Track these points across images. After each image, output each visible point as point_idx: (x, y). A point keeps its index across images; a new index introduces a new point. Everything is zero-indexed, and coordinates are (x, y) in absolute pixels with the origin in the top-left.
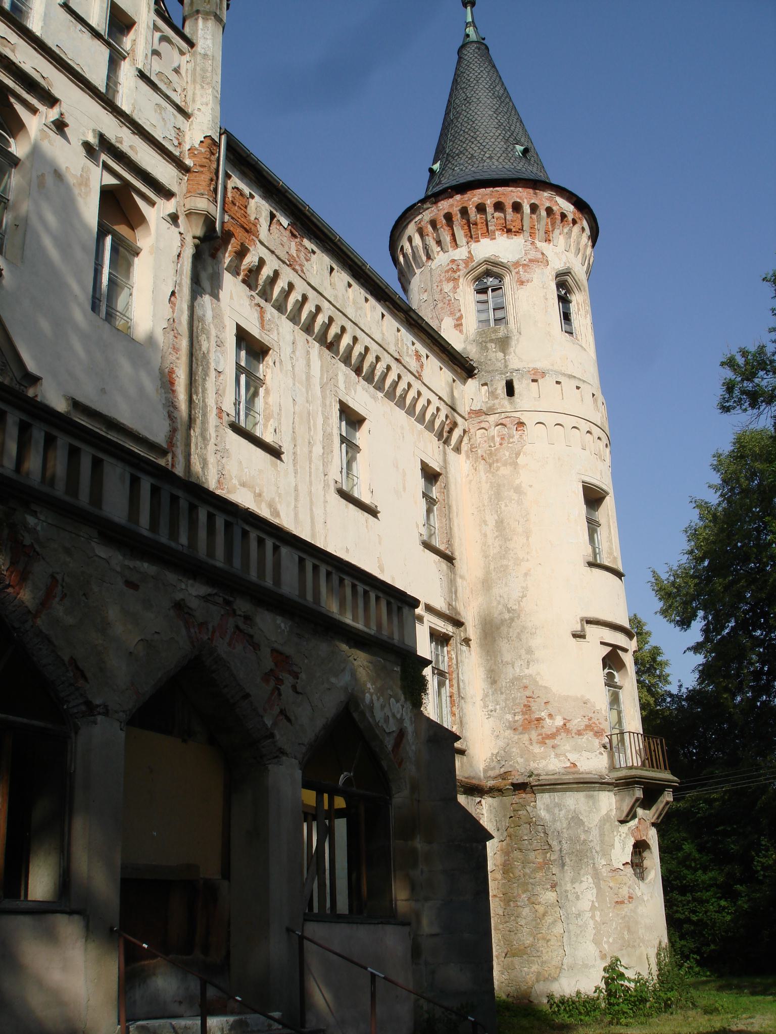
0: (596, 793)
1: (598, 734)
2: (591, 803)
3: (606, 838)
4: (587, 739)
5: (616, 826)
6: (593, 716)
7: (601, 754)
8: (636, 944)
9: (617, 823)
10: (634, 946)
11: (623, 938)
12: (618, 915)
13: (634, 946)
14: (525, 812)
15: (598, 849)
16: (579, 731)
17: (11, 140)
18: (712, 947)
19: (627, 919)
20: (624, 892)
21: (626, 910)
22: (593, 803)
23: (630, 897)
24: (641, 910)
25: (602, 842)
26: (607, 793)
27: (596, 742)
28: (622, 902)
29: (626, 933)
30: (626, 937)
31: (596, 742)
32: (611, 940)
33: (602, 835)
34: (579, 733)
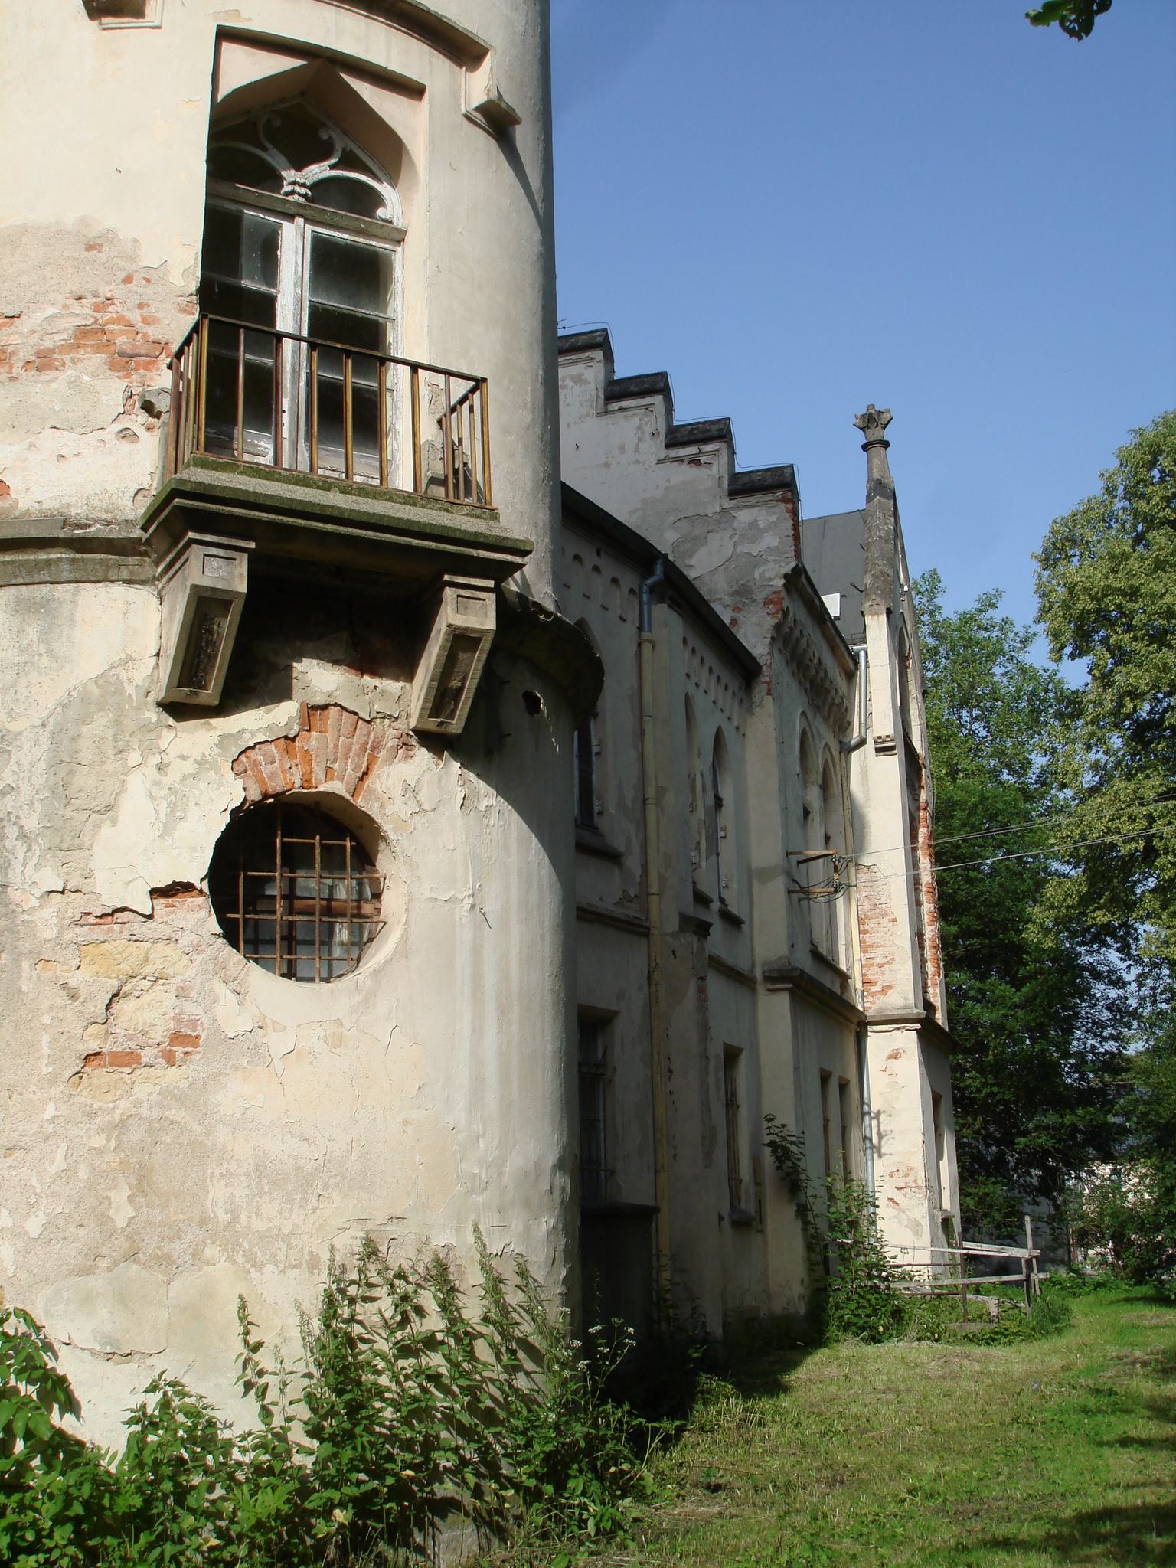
0: (63, 591)
1: (124, 361)
2: (33, 631)
3: (84, 779)
4: (73, 383)
5: (146, 728)
6: (117, 290)
7: (125, 434)
8: (176, 1248)
9: (153, 715)
10: (164, 1260)
11: (103, 1219)
12: (91, 1114)
13: (164, 1260)
14: (1130, 1195)
15: (32, 822)
16: (42, 354)
17: (383, 188)
18: (666, 1275)
19: (136, 1133)
20: (148, 1014)
21: (140, 1091)
22: (45, 635)
23: (177, 1037)
24: (235, 1094)
25: (61, 793)
26: (118, 590)
27: (113, 390)
28: (128, 1059)
29: (120, 1196)
30: (121, 1213)
31: (113, 390)
32: (34, 1226)
33: (63, 762)
34: (43, 361)
